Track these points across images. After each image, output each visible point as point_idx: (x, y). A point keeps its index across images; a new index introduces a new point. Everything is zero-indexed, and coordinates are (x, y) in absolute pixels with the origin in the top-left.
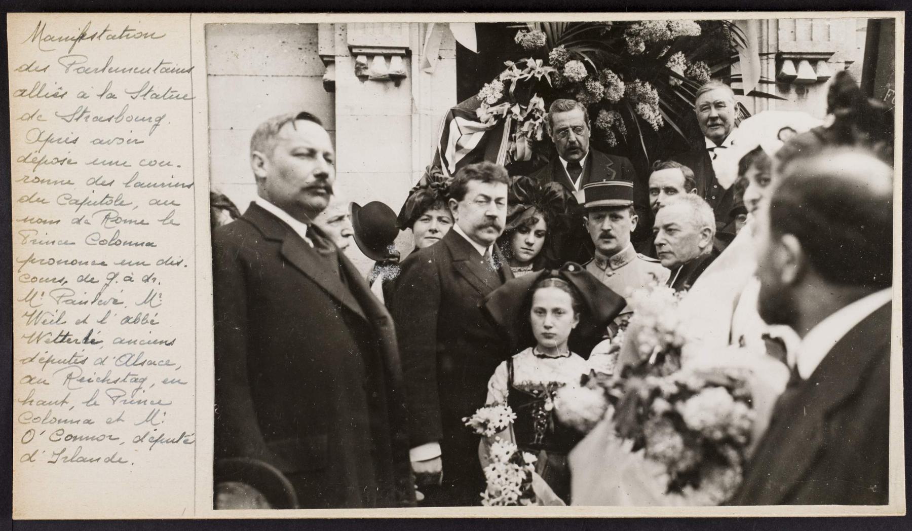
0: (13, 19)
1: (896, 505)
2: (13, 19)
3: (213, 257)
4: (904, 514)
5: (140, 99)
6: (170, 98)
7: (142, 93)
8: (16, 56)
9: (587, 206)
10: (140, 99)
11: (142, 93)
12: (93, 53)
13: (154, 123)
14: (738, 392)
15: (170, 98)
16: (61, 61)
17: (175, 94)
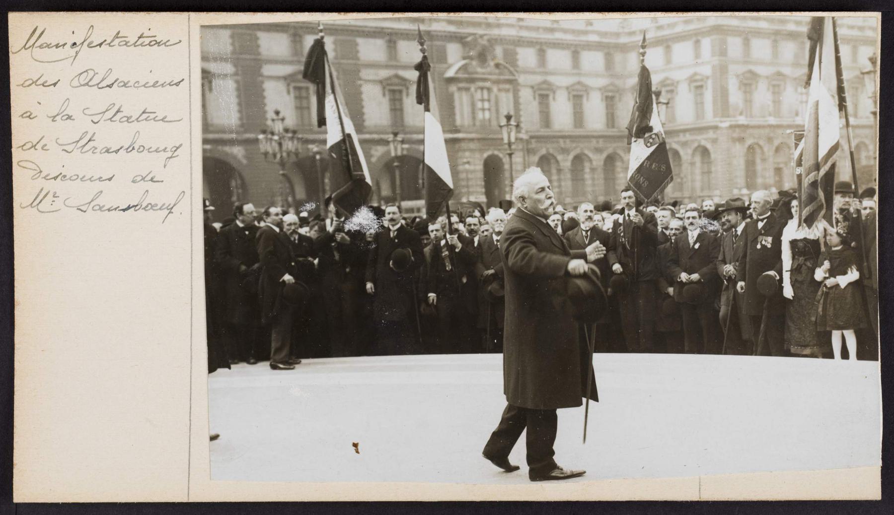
8: (20, 66)
11: (80, 144)
12: (96, 60)
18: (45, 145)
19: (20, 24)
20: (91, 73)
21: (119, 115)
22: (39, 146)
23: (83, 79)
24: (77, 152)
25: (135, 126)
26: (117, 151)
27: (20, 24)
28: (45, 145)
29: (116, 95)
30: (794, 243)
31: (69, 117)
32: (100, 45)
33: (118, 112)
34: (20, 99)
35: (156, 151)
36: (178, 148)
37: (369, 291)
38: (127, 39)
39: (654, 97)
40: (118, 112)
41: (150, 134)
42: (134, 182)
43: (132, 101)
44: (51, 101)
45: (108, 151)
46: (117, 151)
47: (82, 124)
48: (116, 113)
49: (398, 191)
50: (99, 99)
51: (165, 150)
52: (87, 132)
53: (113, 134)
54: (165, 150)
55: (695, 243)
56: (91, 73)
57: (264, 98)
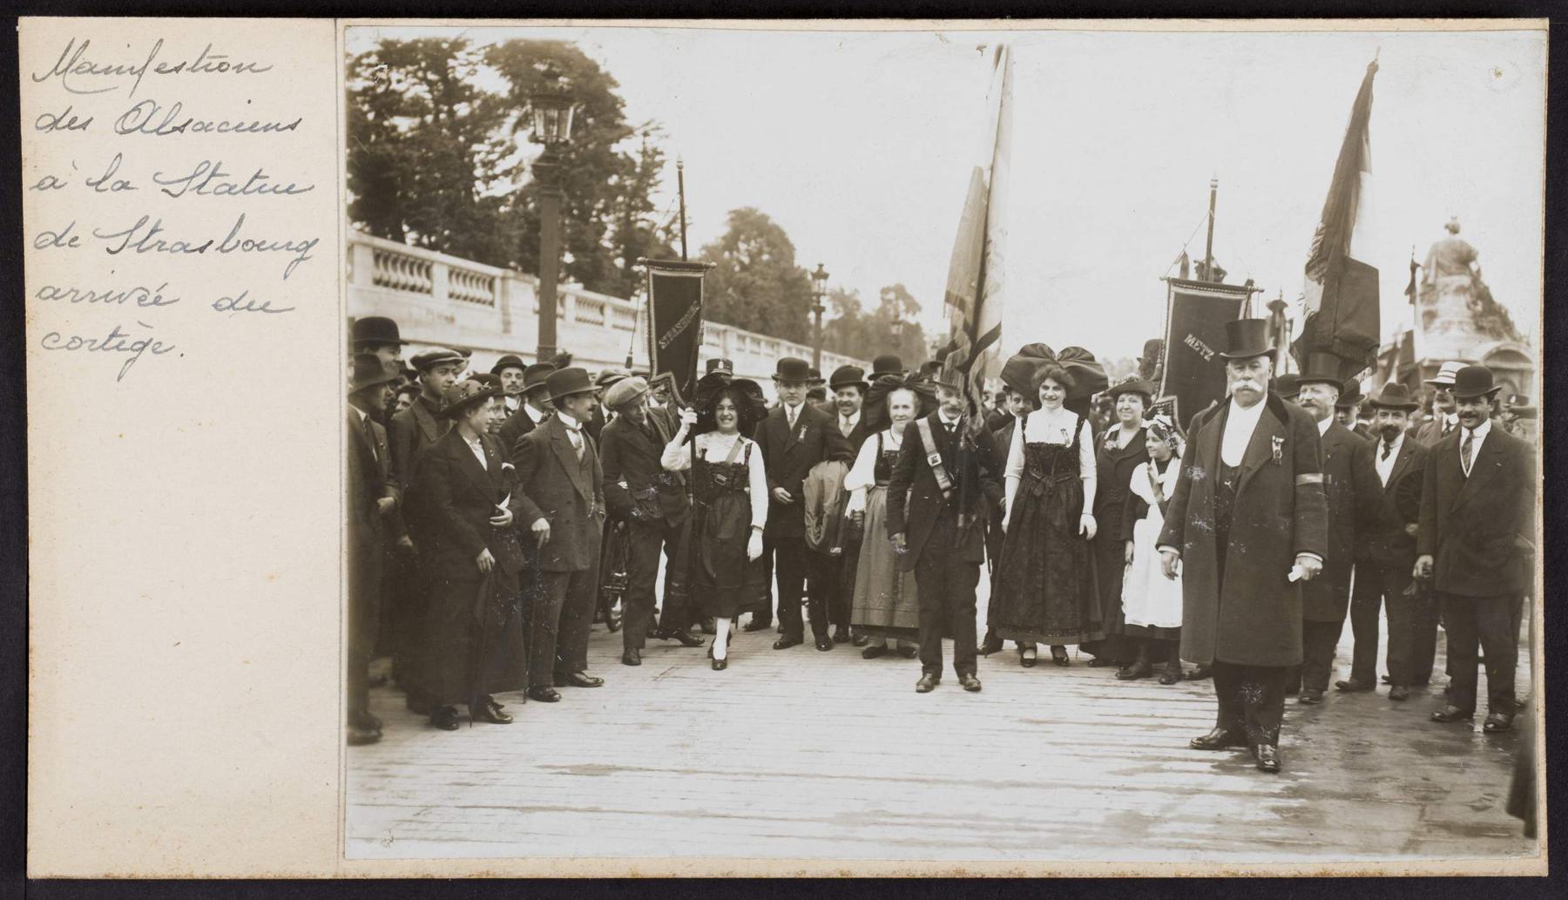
8: (37, 99)
11: (197, 181)
18: (76, 238)
19: (39, 37)
21: (215, 181)
22: (65, 240)
24: (190, 196)
27: (39, 37)
28: (76, 238)
30: (1032, 450)
31: (125, 186)
32: (177, 69)
33: (152, 232)
34: (41, 152)
36: (309, 246)
37: (666, 460)
40: (152, 232)
42: (216, 306)
46: (202, 250)
48: (206, 178)
50: (181, 155)
52: (147, 217)
53: (206, 216)
54: (288, 246)
55: (1382, 357)
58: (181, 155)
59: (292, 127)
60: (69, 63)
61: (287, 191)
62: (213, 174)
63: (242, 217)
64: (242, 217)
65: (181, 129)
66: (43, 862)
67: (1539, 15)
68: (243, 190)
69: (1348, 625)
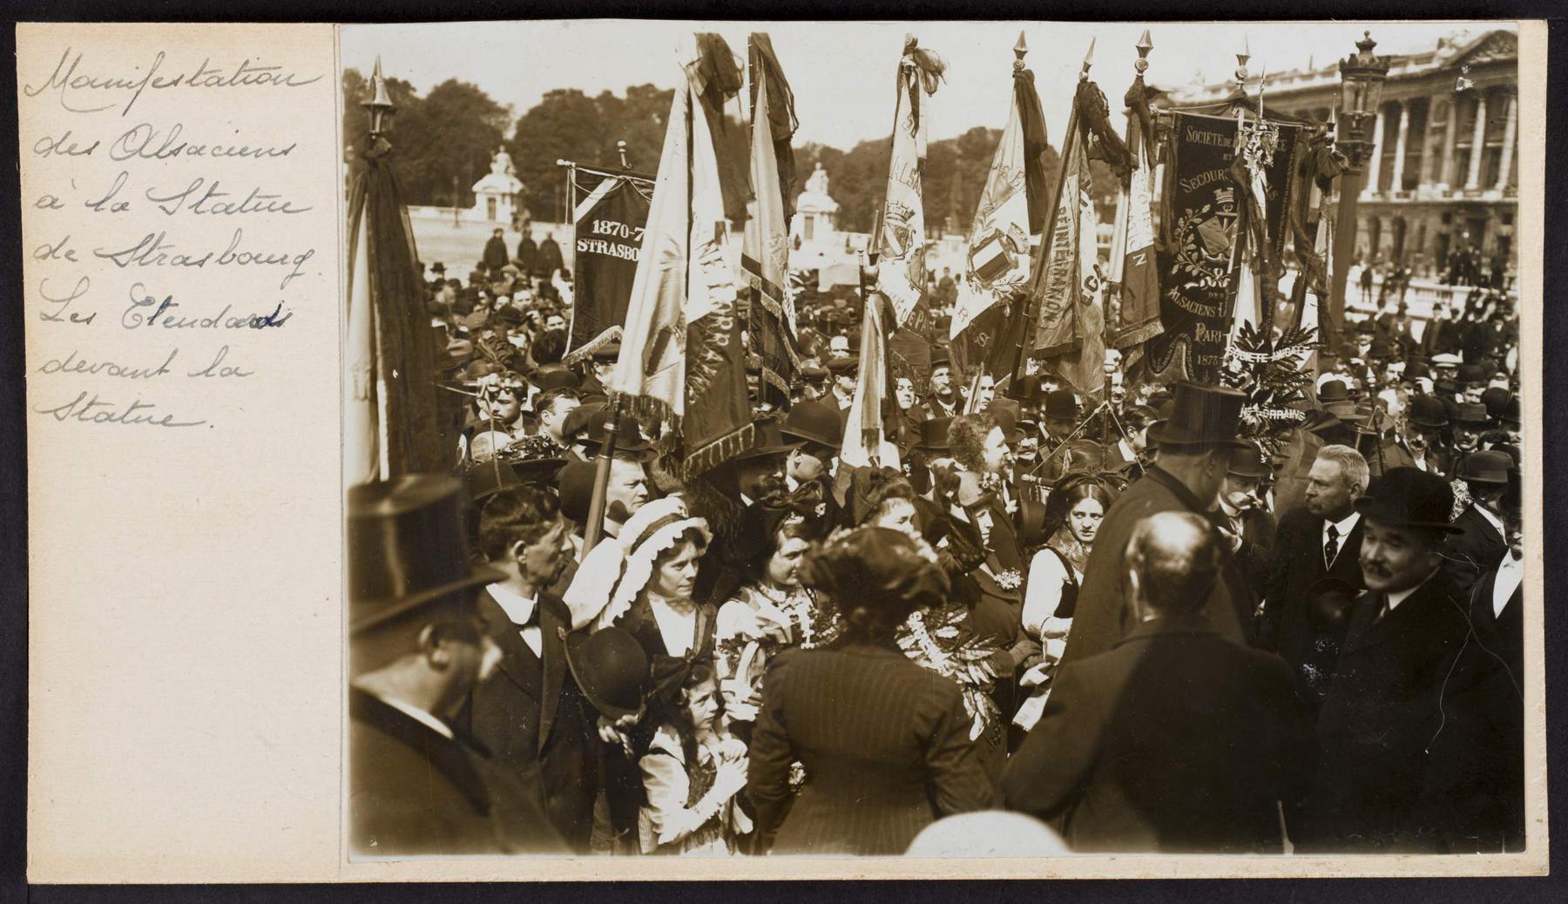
0: (27, 33)
1: (1532, 858)
2: (27, 33)
3: (1327, 17)
4: (1547, 874)
5: (184, 213)
6: (255, 209)
7: (192, 199)
8: (37, 117)
9: (835, 461)
10: (184, 213)
11: (192, 199)
12: (162, 111)
13: (290, 268)
14: (1144, 45)
15: (255, 209)
16: (146, 129)
17: (266, 203)
18: (72, 252)
19: (38, 45)
20: (143, 133)
21: (211, 201)
22: (61, 252)
23: (133, 144)
25: (238, 219)
26: (201, 263)
27: (38, 45)
28: (72, 252)
29: (209, 168)
32: (175, 83)
34: (37, 175)
35: (268, 261)
38: (219, 74)
39: (1362, 223)
41: (264, 233)
43: (237, 180)
44: (98, 174)
45: (185, 262)
46: (201, 263)
47: (143, 219)
49: (602, 247)
50: (173, 175)
51: (283, 260)
53: (195, 232)
54: (283, 260)
56: (143, 133)
57: (484, 95)
58: (173, 175)
59: (285, 152)
60: (66, 77)
61: (163, 423)
62: (209, 195)
63: (175, 352)
64: (175, 352)
65: (174, 153)
66: (37, 874)
67: (1542, 18)
68: (122, 418)
69: (1339, 548)
